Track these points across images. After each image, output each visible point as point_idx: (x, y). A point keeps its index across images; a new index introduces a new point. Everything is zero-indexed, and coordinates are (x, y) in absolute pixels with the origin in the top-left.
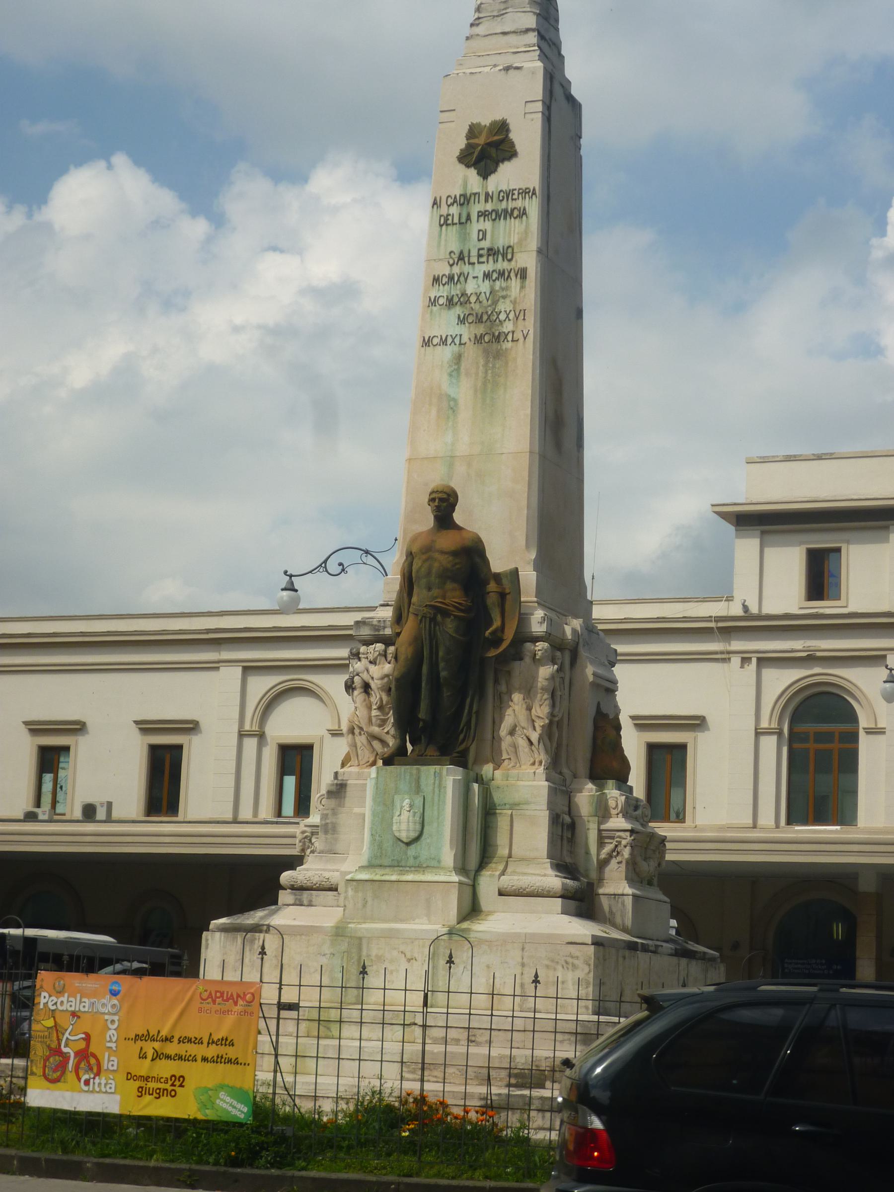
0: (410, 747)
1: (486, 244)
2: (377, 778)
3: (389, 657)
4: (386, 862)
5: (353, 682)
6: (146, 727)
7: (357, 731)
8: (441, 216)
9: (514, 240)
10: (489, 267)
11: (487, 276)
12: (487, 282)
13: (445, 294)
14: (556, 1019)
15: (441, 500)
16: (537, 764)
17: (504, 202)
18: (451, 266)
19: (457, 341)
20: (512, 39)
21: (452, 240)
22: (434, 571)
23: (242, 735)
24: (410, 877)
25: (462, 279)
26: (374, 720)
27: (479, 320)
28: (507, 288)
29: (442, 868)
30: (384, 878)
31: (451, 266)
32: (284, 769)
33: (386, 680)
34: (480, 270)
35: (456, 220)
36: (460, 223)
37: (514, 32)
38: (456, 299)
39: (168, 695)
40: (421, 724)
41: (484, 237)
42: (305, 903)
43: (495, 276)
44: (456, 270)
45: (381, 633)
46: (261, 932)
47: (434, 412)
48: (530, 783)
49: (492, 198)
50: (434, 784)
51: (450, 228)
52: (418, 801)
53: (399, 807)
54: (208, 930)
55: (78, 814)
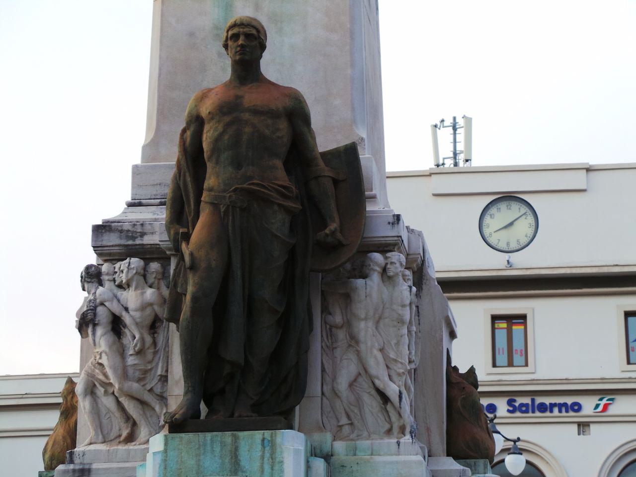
0: (203, 408)
2: (166, 451)
3: (151, 279)
5: (95, 315)
7: (100, 390)
15: (248, 36)
16: (396, 430)
22: (245, 137)
26: (131, 371)
33: (148, 311)
40: (227, 369)
45: (138, 242)
48: (394, 458)
50: (263, 457)
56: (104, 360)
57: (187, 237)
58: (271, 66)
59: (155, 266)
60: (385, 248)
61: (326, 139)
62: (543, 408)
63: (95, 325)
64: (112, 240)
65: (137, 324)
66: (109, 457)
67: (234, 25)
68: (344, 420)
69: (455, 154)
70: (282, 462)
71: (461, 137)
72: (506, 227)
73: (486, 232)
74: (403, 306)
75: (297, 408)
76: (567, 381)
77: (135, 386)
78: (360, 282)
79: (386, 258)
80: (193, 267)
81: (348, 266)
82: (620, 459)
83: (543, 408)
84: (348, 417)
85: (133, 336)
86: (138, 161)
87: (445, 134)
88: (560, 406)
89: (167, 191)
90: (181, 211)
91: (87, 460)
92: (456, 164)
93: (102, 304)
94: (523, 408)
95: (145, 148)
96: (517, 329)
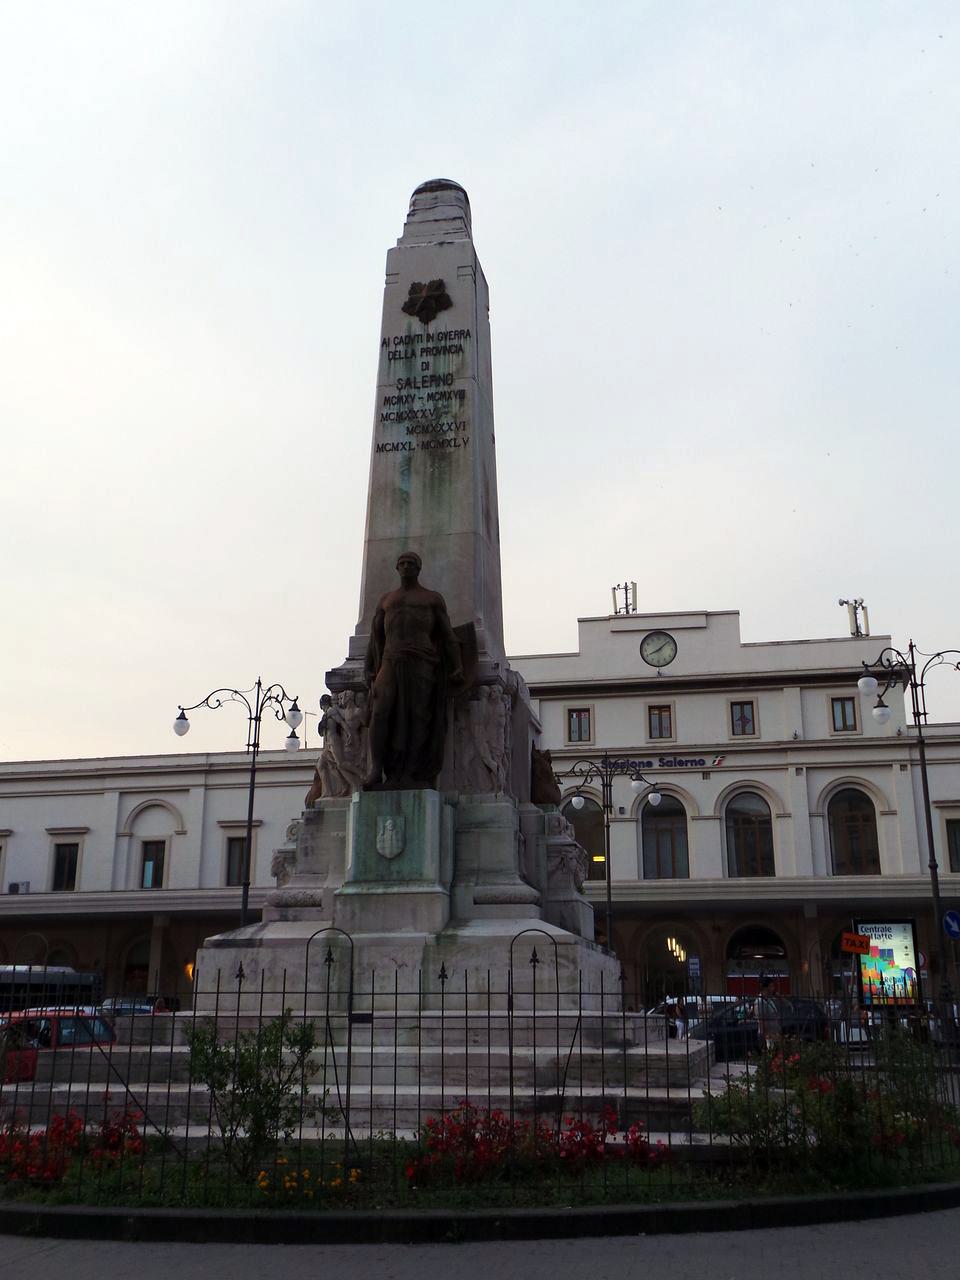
0: (384, 776)
1: (429, 373)
4: (371, 876)
6: (53, 832)
7: (330, 767)
8: (390, 352)
9: (453, 369)
10: (433, 390)
11: (431, 397)
12: (431, 402)
13: (395, 411)
14: (489, 1017)
15: (409, 563)
16: (496, 788)
17: (443, 342)
18: (400, 390)
19: (407, 447)
20: (444, 225)
21: (400, 370)
23: (118, 836)
24: (395, 890)
25: (410, 400)
27: (425, 430)
28: (448, 406)
29: (425, 881)
30: (371, 891)
31: (400, 390)
32: (145, 858)
34: (424, 392)
35: (403, 355)
36: (406, 358)
37: (445, 220)
38: (405, 415)
39: (67, 812)
41: (427, 368)
42: (291, 918)
43: (437, 397)
44: (404, 393)
46: (253, 946)
47: (389, 503)
48: (493, 805)
49: (432, 338)
51: (397, 361)
52: (400, 821)
53: (381, 827)
54: (202, 947)
55: (6, 890)
56: (332, 750)
57: (374, 678)
58: (425, 579)
59: (360, 695)
60: (490, 683)
61: (455, 619)
62: (681, 763)
63: (327, 729)
64: (336, 680)
65: (350, 728)
66: (334, 804)
67: (402, 557)
68: (466, 783)
69: (627, 606)
70: (424, 807)
71: (630, 595)
72: (657, 651)
73: (645, 654)
74: (501, 716)
75: (439, 776)
76: (696, 746)
77: (349, 764)
78: (476, 702)
79: (491, 688)
80: (376, 696)
81: (470, 694)
82: (839, 785)
83: (681, 763)
84: (469, 781)
85: (348, 735)
86: (353, 634)
87: (620, 594)
88: (692, 762)
89: (365, 651)
90: (371, 665)
91: (322, 806)
92: (627, 612)
93: (330, 717)
94: (669, 764)
95: (357, 626)
96: (665, 714)
